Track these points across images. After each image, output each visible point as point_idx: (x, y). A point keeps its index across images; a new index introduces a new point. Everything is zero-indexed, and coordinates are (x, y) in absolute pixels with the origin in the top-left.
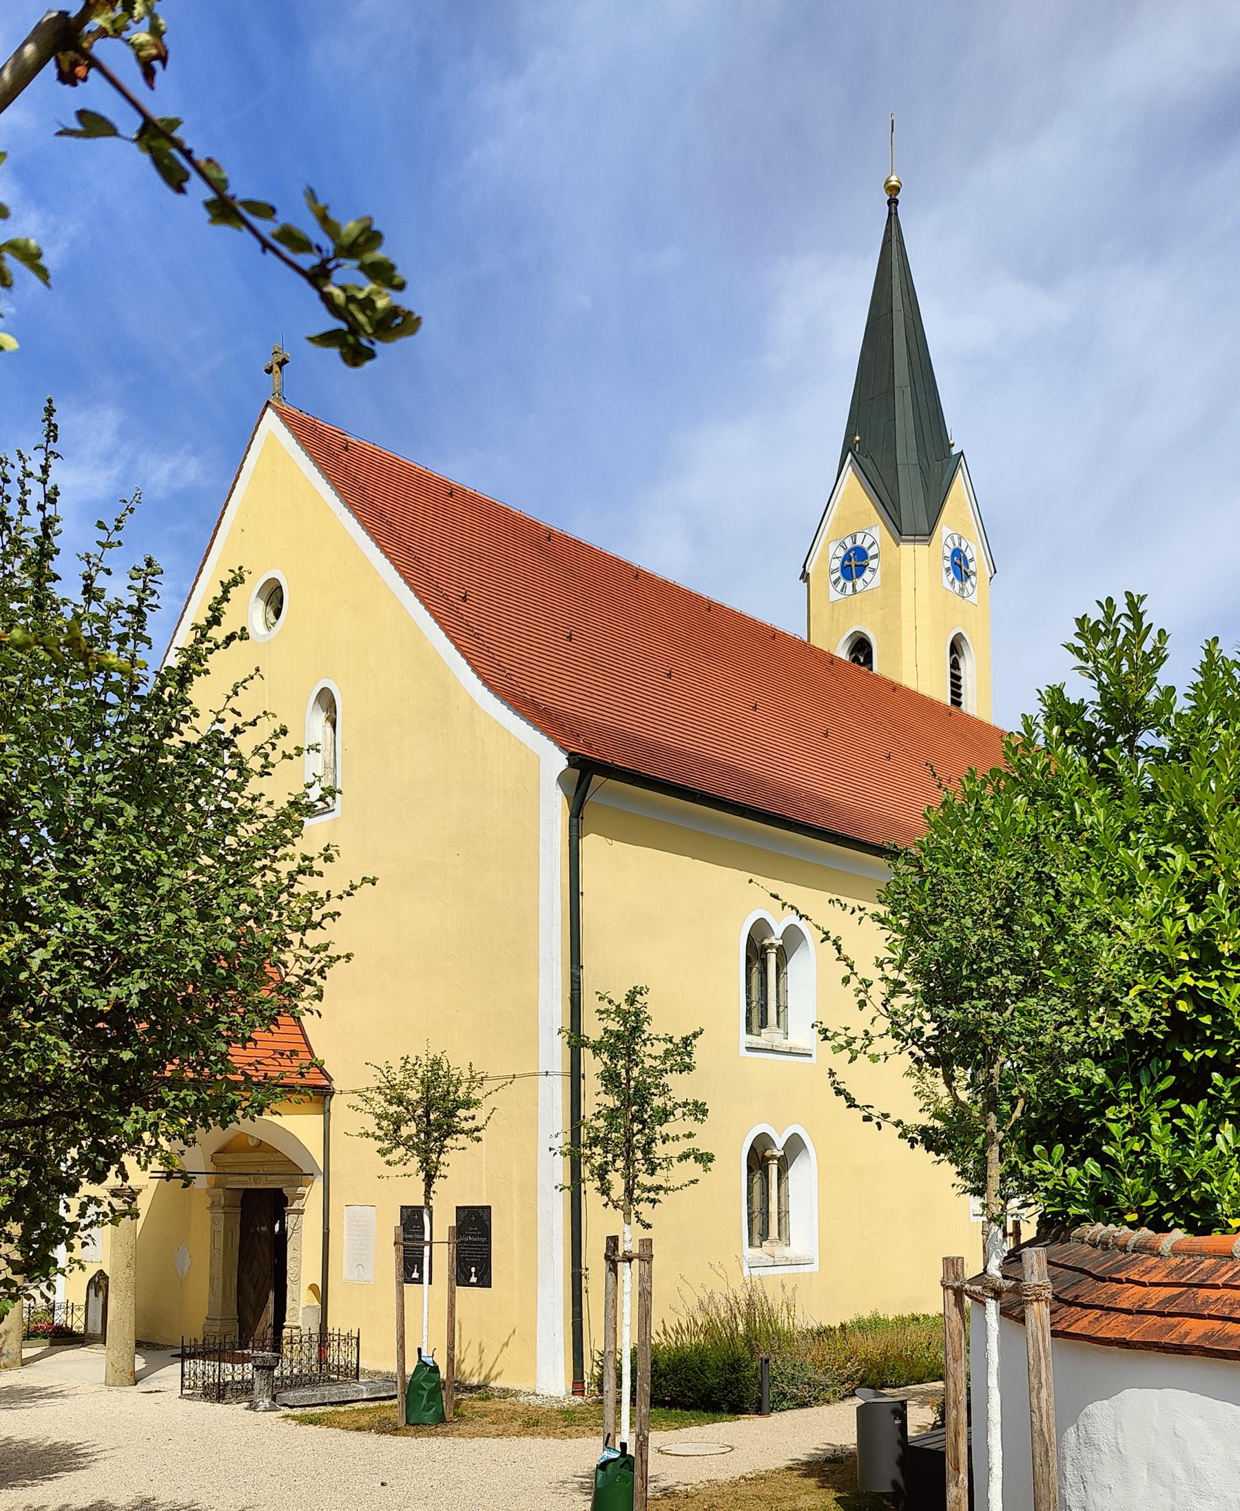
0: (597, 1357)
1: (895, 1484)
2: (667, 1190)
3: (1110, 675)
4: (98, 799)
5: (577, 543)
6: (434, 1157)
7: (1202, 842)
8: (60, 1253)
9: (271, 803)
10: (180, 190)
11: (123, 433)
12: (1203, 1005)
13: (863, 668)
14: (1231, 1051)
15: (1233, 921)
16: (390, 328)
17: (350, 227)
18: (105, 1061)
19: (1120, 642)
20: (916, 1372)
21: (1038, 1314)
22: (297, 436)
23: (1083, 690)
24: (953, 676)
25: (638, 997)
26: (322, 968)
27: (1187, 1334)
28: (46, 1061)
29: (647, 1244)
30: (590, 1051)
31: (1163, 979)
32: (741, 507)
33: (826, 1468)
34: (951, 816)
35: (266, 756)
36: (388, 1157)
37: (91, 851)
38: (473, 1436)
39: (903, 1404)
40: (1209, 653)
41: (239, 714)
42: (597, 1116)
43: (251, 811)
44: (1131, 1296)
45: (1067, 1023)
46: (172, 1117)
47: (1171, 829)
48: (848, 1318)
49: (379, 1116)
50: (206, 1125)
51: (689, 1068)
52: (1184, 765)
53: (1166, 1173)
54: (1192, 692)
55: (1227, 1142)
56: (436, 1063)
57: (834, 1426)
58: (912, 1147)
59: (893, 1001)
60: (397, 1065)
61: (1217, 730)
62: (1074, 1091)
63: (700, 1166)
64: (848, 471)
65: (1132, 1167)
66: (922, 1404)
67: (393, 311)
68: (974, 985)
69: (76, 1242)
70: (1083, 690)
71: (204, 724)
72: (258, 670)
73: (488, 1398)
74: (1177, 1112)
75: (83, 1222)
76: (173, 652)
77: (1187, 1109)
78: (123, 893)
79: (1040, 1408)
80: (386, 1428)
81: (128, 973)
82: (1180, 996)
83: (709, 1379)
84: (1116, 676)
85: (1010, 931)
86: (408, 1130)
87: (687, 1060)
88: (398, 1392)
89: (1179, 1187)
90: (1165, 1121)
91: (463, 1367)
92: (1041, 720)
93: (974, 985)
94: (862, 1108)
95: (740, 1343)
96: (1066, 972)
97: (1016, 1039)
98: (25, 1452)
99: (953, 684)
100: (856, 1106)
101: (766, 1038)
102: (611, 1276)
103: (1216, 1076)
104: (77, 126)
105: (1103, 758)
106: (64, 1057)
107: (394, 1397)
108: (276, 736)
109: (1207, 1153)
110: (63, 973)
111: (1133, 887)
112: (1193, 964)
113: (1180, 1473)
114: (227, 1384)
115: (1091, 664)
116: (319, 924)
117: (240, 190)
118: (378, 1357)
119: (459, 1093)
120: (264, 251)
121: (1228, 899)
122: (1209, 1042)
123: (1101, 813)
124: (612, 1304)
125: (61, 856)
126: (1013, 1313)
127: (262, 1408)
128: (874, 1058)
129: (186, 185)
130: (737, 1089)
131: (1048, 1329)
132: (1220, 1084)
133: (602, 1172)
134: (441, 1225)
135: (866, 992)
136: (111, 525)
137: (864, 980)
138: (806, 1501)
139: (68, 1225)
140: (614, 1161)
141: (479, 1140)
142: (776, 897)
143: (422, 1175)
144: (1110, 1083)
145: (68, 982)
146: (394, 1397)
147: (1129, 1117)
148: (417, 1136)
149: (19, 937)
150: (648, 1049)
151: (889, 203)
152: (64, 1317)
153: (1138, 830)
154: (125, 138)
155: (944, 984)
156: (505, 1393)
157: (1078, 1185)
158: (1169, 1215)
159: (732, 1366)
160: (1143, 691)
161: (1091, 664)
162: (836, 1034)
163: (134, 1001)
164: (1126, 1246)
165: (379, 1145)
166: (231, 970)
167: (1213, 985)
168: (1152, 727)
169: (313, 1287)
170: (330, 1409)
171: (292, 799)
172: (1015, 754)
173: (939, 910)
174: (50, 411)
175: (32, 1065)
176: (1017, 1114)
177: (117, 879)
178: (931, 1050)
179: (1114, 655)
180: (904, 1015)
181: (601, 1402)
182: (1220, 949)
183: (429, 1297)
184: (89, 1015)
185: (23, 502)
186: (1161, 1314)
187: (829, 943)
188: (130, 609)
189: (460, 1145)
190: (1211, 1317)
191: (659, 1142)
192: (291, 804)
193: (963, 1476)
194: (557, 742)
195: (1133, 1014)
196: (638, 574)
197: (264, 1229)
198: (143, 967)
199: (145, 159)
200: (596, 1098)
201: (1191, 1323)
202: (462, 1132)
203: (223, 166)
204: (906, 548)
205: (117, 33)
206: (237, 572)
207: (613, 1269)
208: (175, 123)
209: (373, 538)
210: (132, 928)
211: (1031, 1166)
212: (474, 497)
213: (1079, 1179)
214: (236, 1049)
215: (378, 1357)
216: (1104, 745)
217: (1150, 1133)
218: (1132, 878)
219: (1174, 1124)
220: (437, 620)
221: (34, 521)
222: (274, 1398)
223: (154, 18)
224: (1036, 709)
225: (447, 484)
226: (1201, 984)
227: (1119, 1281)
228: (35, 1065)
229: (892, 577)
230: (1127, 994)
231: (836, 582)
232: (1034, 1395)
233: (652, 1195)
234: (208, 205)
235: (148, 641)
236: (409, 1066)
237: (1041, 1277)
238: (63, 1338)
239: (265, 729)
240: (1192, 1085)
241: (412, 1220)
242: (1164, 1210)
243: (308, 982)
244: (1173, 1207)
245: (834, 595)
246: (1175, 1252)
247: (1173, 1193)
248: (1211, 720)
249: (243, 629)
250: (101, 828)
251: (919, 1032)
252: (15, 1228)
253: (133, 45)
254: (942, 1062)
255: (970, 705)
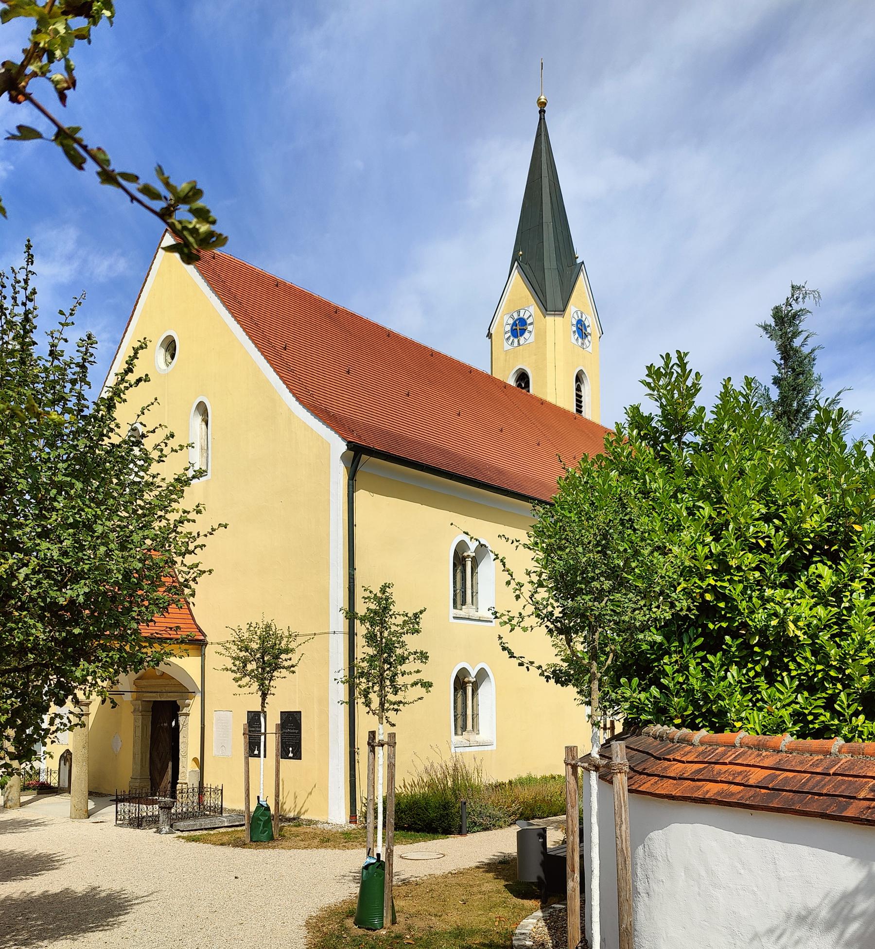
0: (364, 801)
1: (539, 878)
2: (404, 704)
3: (667, 400)
4: (60, 478)
5: (353, 315)
6: (267, 682)
7: (720, 500)
8: (37, 747)
9: (164, 479)
10: (81, 168)
11: (79, 242)
12: (721, 596)
13: (524, 391)
14: (737, 624)
15: (738, 547)
16: (208, 243)
17: (183, 186)
18: (64, 634)
19: (673, 379)
20: (555, 809)
21: (621, 780)
23: (651, 408)
24: (577, 395)
25: (387, 589)
26: (195, 578)
27: (708, 792)
28: (29, 634)
29: (392, 736)
30: (359, 621)
31: (697, 581)
32: (450, 294)
33: (500, 867)
34: (571, 484)
35: (162, 450)
36: (239, 683)
37: (54, 509)
38: (290, 848)
39: (544, 830)
40: (725, 386)
41: (145, 426)
42: (363, 660)
43: (152, 483)
44: (676, 769)
45: (638, 609)
46: (105, 667)
47: (702, 492)
48: (513, 777)
49: (234, 658)
50: (126, 671)
51: (418, 631)
52: (710, 453)
53: (698, 695)
54: (715, 410)
55: (733, 677)
56: (268, 626)
57: (504, 842)
58: (547, 681)
59: (536, 595)
60: (245, 628)
61: (729, 433)
62: (645, 647)
63: (424, 690)
64: (515, 273)
65: (678, 692)
66: (557, 828)
67: (211, 234)
68: (584, 587)
69: (48, 740)
70: (651, 408)
71: (124, 432)
72: (156, 399)
73: (300, 826)
74: (704, 659)
75: (53, 728)
76: (105, 389)
77: (710, 657)
78: (75, 534)
79: (621, 836)
80: (238, 844)
81: (78, 583)
82: (706, 591)
83: (429, 814)
84: (671, 401)
85: (605, 554)
86: (252, 666)
87: (416, 626)
88: (246, 822)
89: (706, 703)
90: (698, 664)
91: (285, 807)
92: (626, 425)
93: (584, 587)
94: (518, 658)
95: (449, 793)
96: (640, 577)
97: (608, 618)
98: (22, 859)
99: (577, 400)
100: (514, 657)
101: (465, 611)
102: (371, 755)
103: (727, 638)
104: (17, 133)
105: (663, 449)
106: (40, 632)
107: (243, 825)
108: (168, 438)
109: (722, 683)
110: (39, 583)
111: (680, 525)
112: (714, 572)
113: (703, 873)
114: (144, 817)
115: (656, 392)
116: (193, 551)
117: (116, 166)
118: (234, 801)
119: (282, 645)
120: (132, 201)
121: (735, 534)
122: (723, 618)
123: (661, 481)
124: (372, 770)
125: (37, 512)
126: (606, 777)
127: (164, 832)
128: (525, 629)
129: (84, 166)
130: (448, 641)
131: (626, 788)
132: (730, 643)
133: (366, 693)
134: (271, 723)
135: (520, 590)
136: (67, 313)
137: (519, 583)
138: (487, 887)
139: (43, 730)
140: (373, 687)
141: (294, 672)
142: (467, 534)
143: (260, 693)
144: (665, 642)
145: (41, 588)
146: (243, 825)
147: (676, 662)
148: (257, 670)
149: (11, 561)
150: (393, 620)
151: (540, 112)
152: (46, 777)
153: (683, 491)
154: (47, 139)
155: (566, 583)
156: (310, 822)
157: (647, 702)
158: (700, 720)
159: (444, 806)
160: (686, 409)
161: (656, 392)
162: (503, 615)
163: (81, 599)
164: (673, 739)
165: (234, 675)
166: (140, 580)
167: (726, 584)
168: (691, 430)
169: (195, 759)
170: (205, 832)
171: (176, 477)
172: (611, 446)
173: (563, 542)
174: (29, 247)
175: (19, 637)
176: (609, 662)
177: (71, 526)
178: (559, 624)
179: (671, 388)
180: (542, 604)
181: (366, 828)
182: (730, 563)
183: (264, 766)
184: (54, 607)
185: (14, 298)
186: (693, 780)
187: (498, 561)
188: (78, 365)
189: (282, 675)
190: (722, 782)
191: (400, 676)
192: (176, 480)
193: (577, 875)
194: (340, 435)
195: (677, 603)
196: (389, 334)
197: (166, 725)
198: (86, 579)
199: (60, 149)
200: (363, 650)
201: (710, 785)
202: (284, 668)
203: (107, 152)
204: (550, 319)
205: (44, 74)
206: (143, 341)
207: (373, 751)
208: (77, 129)
209: (230, 312)
210: (80, 554)
211: (617, 693)
212: (291, 287)
213: (647, 699)
214: (142, 626)
215: (234, 801)
216: (663, 441)
217: (688, 671)
218: (679, 521)
219: (703, 666)
220: (269, 361)
221: (20, 310)
222: (171, 826)
223: (67, 61)
224: (624, 419)
225: (275, 280)
226: (719, 584)
227: (669, 760)
228: (22, 637)
229: (541, 336)
230: (675, 591)
232: (618, 828)
233: (396, 707)
234: (99, 174)
235: (89, 384)
236: (252, 629)
237: (622, 759)
238: (45, 790)
239: (161, 435)
240: (713, 644)
241: (254, 720)
242: (697, 717)
243: (186, 586)
244: (702, 715)
245: (507, 346)
246: (702, 743)
247: (702, 706)
248: (726, 427)
249: (147, 375)
250: (61, 495)
251: (551, 614)
252: (11, 732)
253: (53, 81)
254: (565, 631)
255: (588, 413)
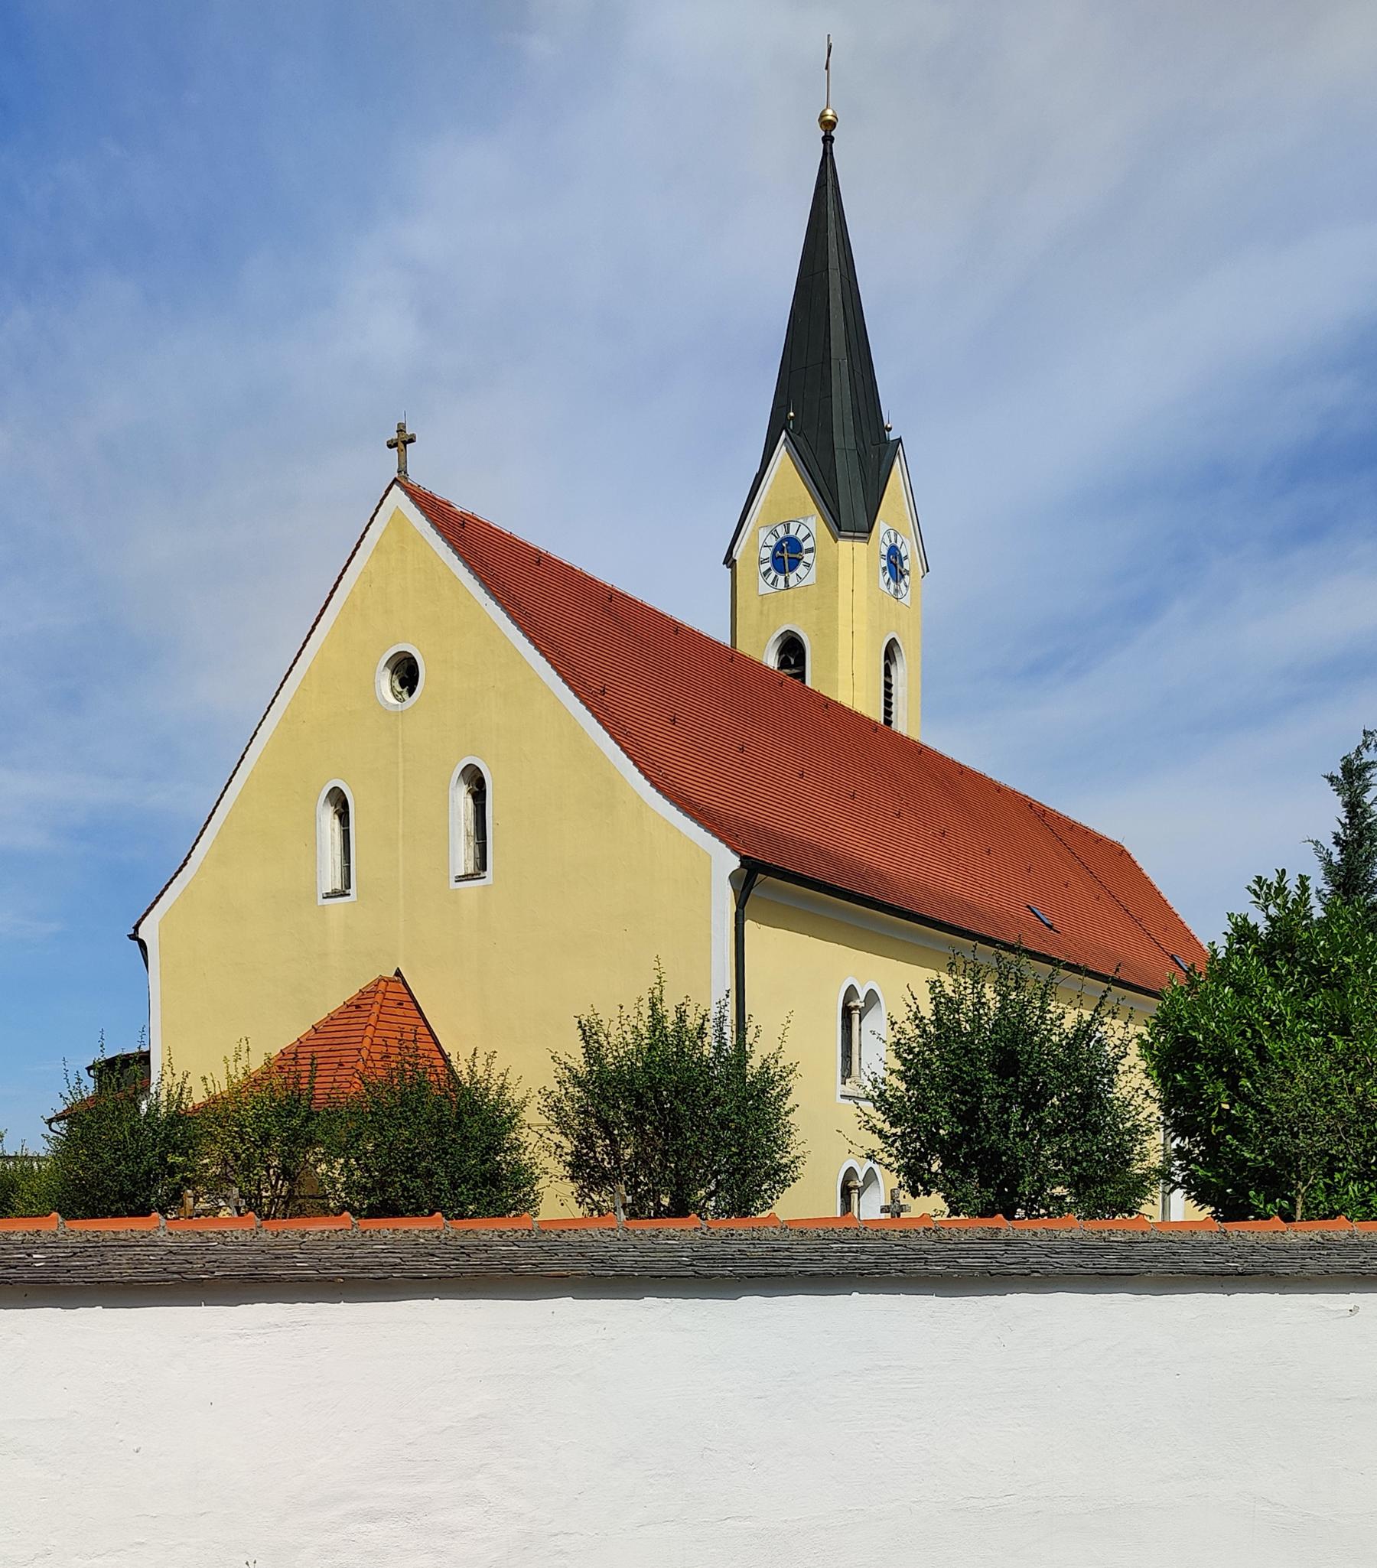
22: (429, 518)
151: (824, 139)
204: (844, 545)
229: (829, 576)
231: (766, 573)
245: (764, 588)
